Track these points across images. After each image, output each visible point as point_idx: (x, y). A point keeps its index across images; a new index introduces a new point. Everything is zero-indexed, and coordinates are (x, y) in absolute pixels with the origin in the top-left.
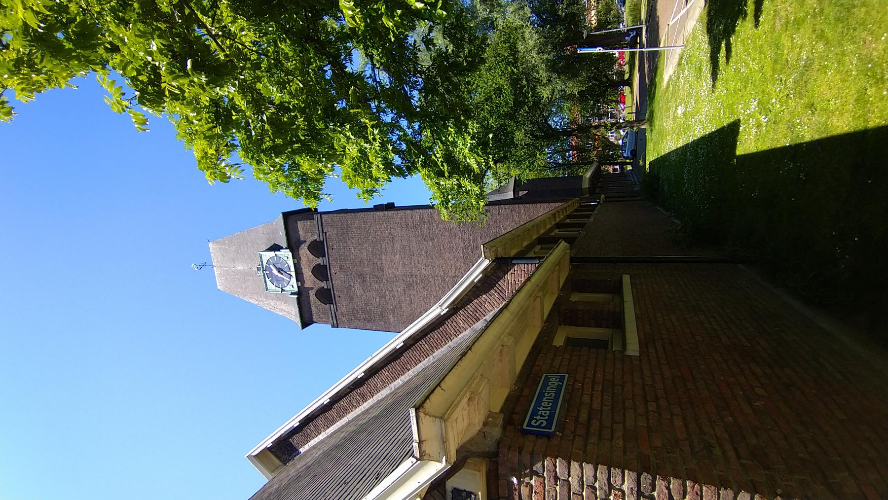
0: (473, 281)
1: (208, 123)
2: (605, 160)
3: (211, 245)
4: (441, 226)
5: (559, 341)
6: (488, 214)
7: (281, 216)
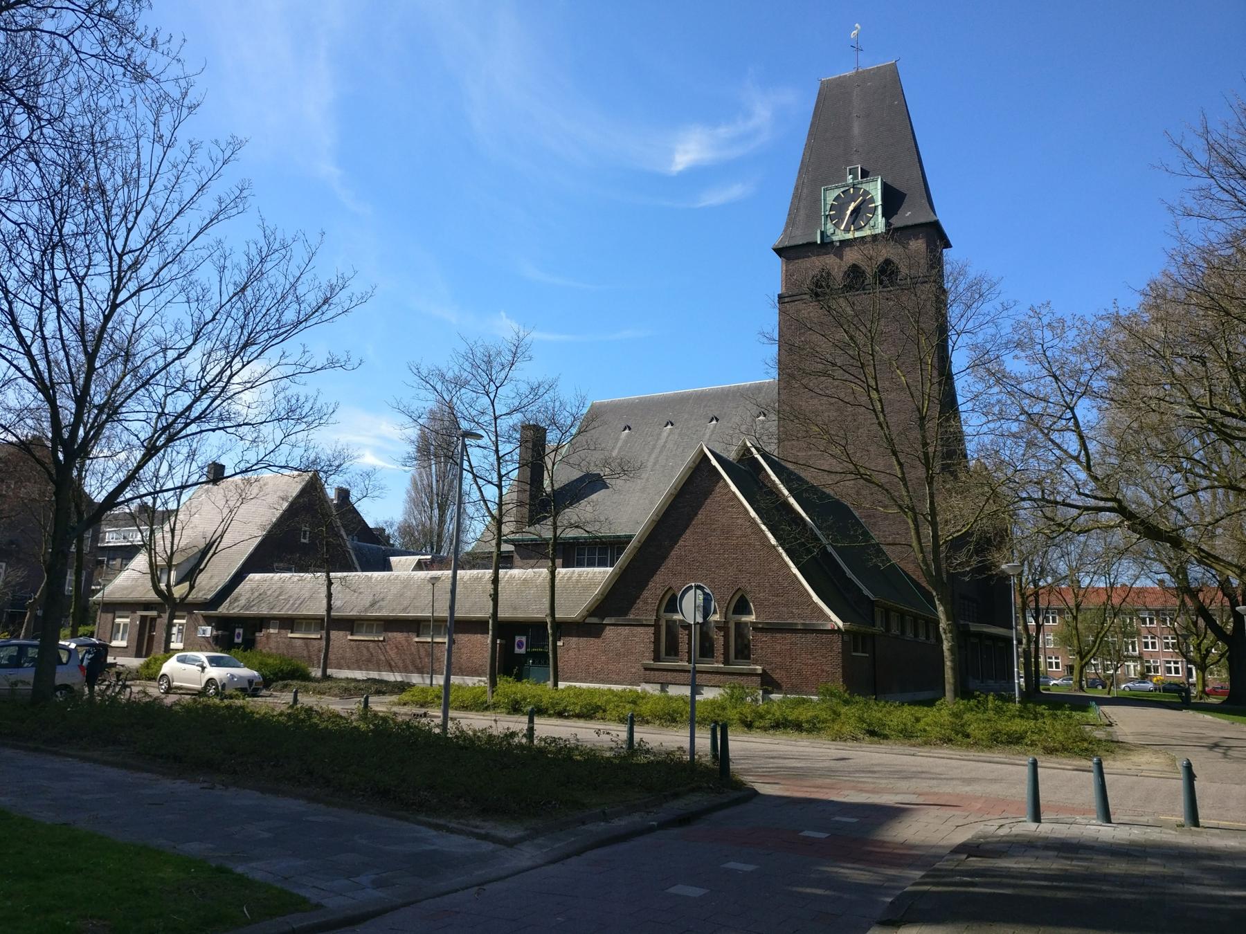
7: (690, 456)
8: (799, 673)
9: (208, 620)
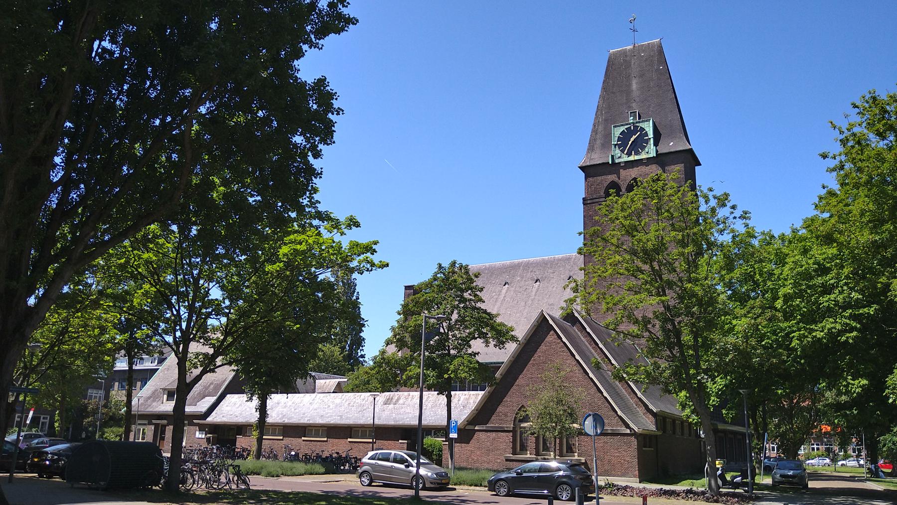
7: (534, 317)
8: (609, 462)
9: (202, 428)
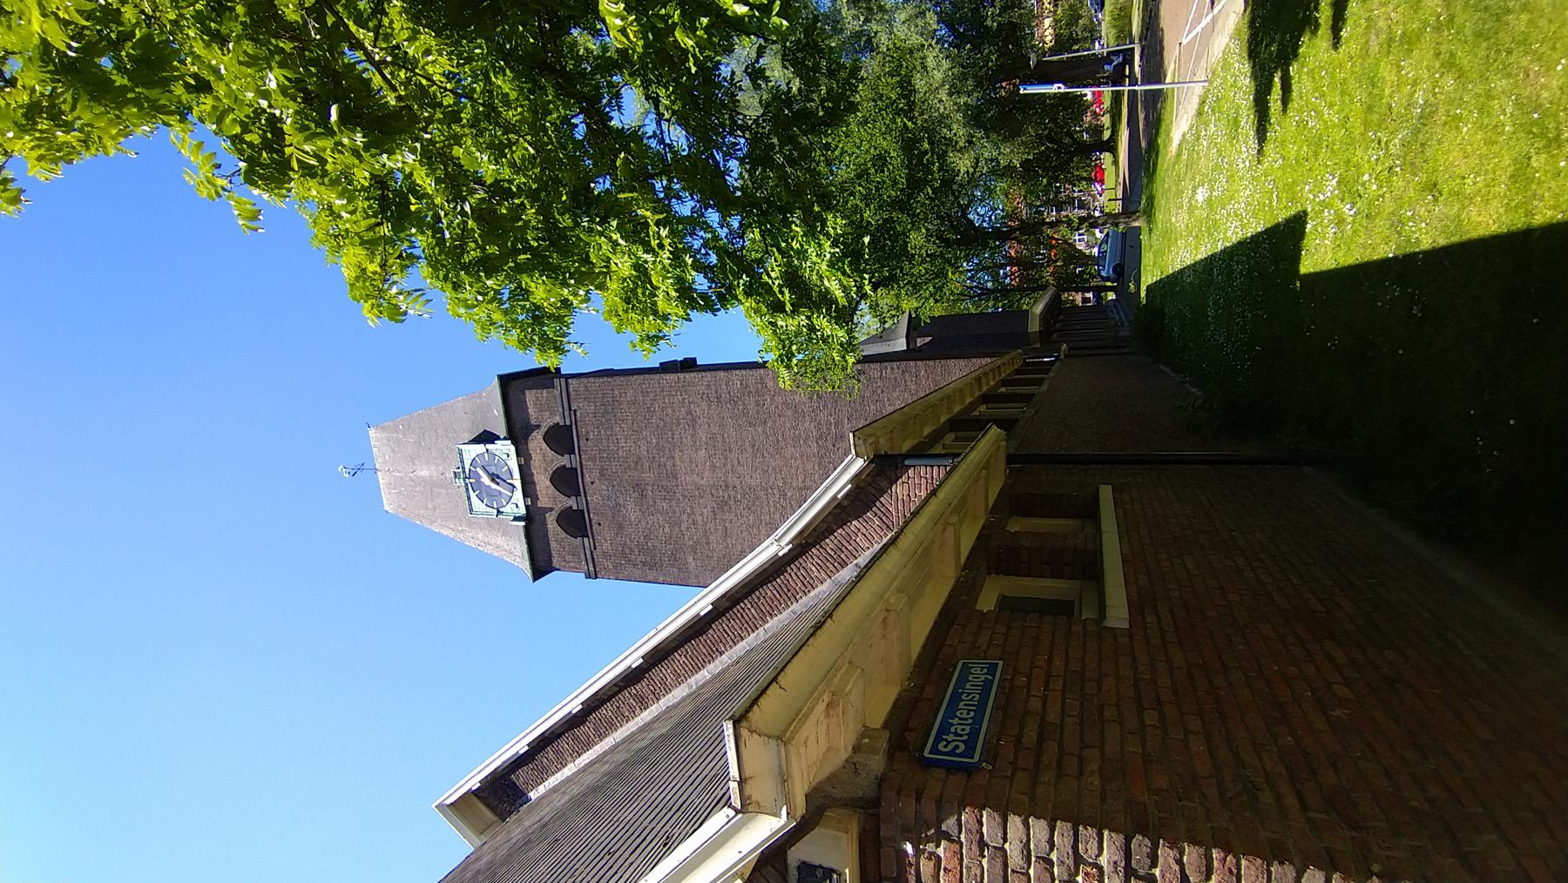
0: (835, 496)
1: (368, 217)
2: (1068, 282)
3: (372, 433)
4: (778, 399)
5: (987, 602)
6: (862, 378)
7: (496, 382)
